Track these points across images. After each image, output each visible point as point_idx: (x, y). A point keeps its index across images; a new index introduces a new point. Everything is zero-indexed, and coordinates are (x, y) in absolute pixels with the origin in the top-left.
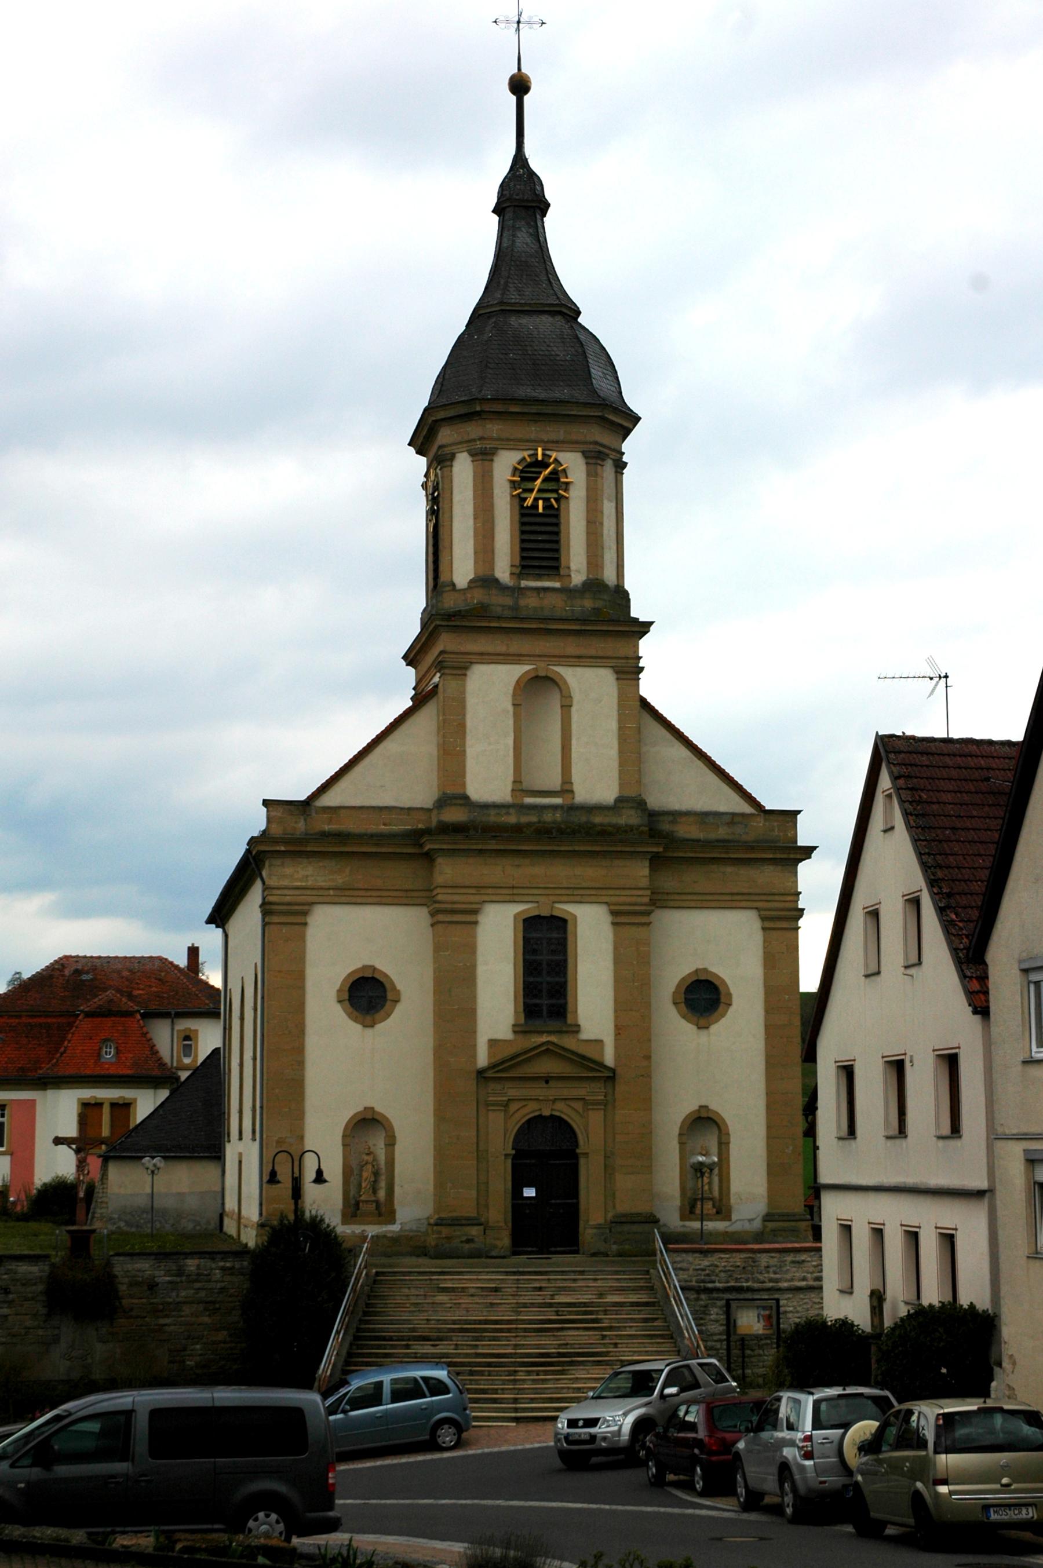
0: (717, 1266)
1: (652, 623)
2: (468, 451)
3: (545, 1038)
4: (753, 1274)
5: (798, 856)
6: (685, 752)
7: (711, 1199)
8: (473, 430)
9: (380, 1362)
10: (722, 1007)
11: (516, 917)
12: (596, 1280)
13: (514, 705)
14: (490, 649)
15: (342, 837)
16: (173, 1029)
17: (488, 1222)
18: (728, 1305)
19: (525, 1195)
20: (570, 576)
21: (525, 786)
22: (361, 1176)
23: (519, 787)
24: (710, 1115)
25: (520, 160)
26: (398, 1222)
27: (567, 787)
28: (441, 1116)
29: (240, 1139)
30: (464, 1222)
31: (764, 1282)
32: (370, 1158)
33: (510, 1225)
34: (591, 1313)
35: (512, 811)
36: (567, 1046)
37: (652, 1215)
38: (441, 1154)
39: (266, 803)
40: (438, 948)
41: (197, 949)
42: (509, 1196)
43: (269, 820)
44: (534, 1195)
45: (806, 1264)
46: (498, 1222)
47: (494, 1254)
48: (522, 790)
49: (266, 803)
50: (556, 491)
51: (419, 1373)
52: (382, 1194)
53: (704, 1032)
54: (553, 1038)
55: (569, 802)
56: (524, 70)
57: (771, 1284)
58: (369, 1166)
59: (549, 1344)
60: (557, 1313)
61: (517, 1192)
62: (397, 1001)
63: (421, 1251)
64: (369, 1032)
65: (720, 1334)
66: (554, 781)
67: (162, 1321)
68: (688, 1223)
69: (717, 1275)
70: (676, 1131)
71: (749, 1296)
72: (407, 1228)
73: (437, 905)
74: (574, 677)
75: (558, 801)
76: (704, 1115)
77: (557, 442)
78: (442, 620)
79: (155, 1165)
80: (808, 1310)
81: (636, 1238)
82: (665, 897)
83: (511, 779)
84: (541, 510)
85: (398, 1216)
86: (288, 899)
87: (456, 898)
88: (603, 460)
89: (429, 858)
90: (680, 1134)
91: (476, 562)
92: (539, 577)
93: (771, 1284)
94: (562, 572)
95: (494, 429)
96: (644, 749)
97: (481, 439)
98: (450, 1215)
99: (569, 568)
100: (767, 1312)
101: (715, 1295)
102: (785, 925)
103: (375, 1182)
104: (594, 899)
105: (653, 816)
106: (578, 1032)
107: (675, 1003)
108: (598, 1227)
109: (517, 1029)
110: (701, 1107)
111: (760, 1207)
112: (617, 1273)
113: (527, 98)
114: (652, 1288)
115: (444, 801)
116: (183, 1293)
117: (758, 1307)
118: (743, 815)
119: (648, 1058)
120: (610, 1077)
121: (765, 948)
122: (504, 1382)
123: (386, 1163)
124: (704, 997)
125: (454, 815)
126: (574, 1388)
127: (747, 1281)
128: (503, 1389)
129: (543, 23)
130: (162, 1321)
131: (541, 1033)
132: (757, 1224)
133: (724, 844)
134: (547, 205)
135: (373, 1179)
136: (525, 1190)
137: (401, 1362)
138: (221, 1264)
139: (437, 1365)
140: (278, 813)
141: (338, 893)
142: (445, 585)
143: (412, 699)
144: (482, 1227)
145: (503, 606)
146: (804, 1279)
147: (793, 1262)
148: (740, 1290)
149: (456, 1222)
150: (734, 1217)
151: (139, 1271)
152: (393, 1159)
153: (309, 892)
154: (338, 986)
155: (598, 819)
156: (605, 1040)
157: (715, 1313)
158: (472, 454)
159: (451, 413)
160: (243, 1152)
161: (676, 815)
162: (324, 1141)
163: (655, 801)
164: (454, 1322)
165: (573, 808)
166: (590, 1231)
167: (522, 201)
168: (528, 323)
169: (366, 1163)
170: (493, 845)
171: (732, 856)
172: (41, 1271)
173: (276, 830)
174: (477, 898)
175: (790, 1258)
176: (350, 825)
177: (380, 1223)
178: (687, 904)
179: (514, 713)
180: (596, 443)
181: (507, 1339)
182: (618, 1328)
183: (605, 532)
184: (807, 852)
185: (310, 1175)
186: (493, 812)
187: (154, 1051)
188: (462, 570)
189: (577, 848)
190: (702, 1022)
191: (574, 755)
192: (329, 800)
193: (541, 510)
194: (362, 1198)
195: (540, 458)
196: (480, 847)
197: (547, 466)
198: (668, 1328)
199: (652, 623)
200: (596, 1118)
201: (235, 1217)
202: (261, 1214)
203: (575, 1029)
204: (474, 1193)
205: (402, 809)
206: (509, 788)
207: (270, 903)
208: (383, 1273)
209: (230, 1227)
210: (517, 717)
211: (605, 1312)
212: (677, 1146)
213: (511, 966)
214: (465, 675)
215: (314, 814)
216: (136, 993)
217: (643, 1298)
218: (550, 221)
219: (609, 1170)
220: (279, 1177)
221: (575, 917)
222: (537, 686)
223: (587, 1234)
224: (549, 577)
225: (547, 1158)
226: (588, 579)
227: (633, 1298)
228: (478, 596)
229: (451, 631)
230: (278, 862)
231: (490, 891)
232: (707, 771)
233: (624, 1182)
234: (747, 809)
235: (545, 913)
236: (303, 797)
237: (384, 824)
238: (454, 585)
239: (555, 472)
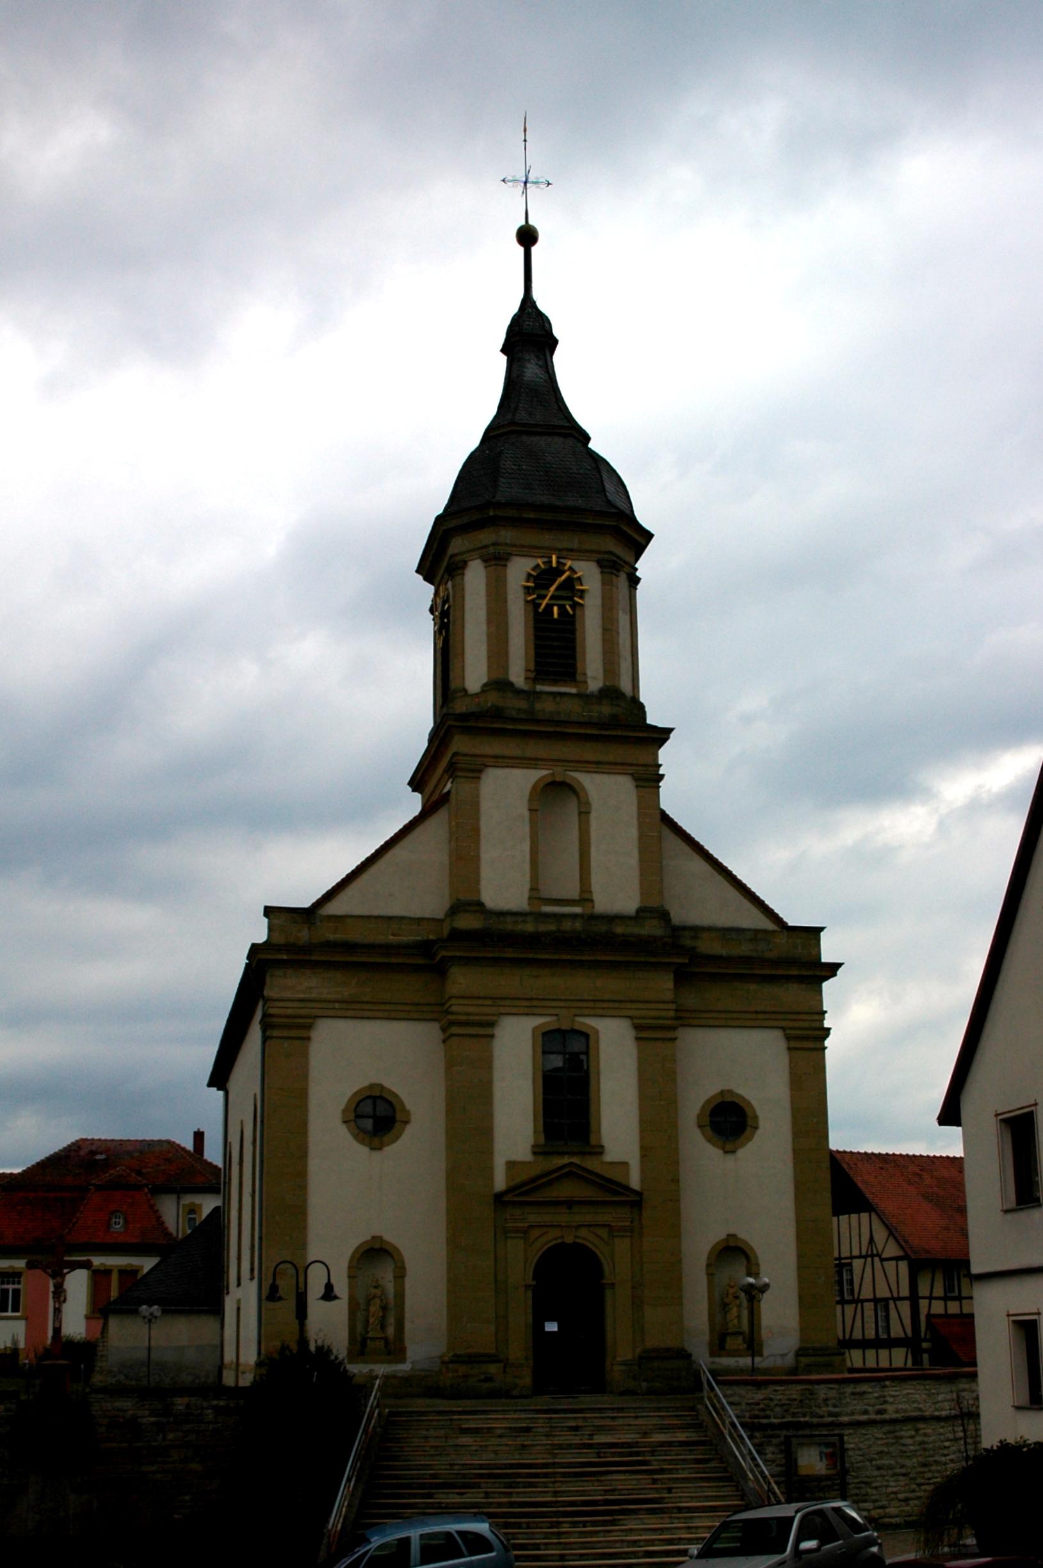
0: (771, 1399)
1: (672, 730)
2: (480, 557)
3: (566, 1160)
4: (810, 1407)
5: (823, 974)
6: (706, 867)
7: (740, 1333)
8: (485, 537)
9: (399, 1514)
10: (748, 1131)
11: (534, 1030)
12: (637, 1417)
13: (530, 810)
14: (506, 752)
15: (350, 947)
16: (178, 1204)
18: (787, 1442)
19: (547, 1329)
20: (586, 682)
21: (545, 894)
22: (367, 1310)
23: (535, 895)
24: (740, 1245)
25: (528, 302)
26: (409, 1361)
27: (586, 896)
28: (453, 1243)
29: (239, 1285)
31: (823, 1417)
32: (378, 1292)
34: (638, 1454)
35: (529, 919)
36: (589, 1167)
37: (683, 1350)
38: (454, 1284)
39: (269, 911)
40: (450, 1064)
41: (203, 1133)
43: (271, 929)
44: (556, 1329)
45: (866, 1396)
47: (515, 1393)
48: (540, 899)
49: (269, 911)
50: (571, 598)
51: (454, 1527)
52: (391, 1331)
53: (730, 1157)
54: (576, 1160)
55: (588, 911)
56: (531, 222)
57: (830, 1419)
58: (377, 1301)
59: (593, 1490)
60: (599, 1455)
61: (538, 1326)
62: (407, 1122)
63: (434, 1391)
64: (376, 1155)
66: (574, 892)
67: (146, 1468)
68: (717, 1360)
70: (703, 1261)
71: (807, 1432)
73: (451, 1017)
74: (594, 785)
75: (577, 910)
76: (732, 1244)
77: (572, 550)
78: (456, 720)
79: (151, 1314)
80: (870, 1446)
81: (669, 1376)
82: (688, 1015)
83: (527, 886)
84: (556, 616)
85: (409, 1354)
86: (289, 1012)
87: (471, 1009)
88: (618, 571)
89: (440, 970)
91: (489, 667)
92: (555, 682)
93: (830, 1419)
94: (579, 678)
95: (507, 535)
96: (664, 862)
97: (494, 544)
98: (468, 1351)
99: (585, 674)
100: (830, 1450)
102: (811, 1045)
103: (383, 1317)
104: (615, 1013)
105: (678, 931)
106: (601, 1153)
107: (700, 1126)
108: (624, 1363)
109: (538, 1150)
110: (729, 1235)
111: (791, 1342)
112: (659, 1409)
113: (534, 250)
115: (457, 908)
116: (171, 1436)
117: (820, 1444)
118: (765, 931)
119: (676, 1181)
120: (635, 1201)
121: (791, 1068)
122: (547, 1535)
123: (395, 1296)
124: (729, 1121)
125: (468, 922)
126: (628, 1541)
127: (804, 1415)
128: (546, 1544)
129: (549, 184)
130: (146, 1468)
131: (562, 1154)
132: (790, 1360)
133: (746, 960)
134: (556, 342)
135: (381, 1314)
136: (546, 1324)
137: (424, 1514)
138: (215, 1402)
139: (477, 1517)
140: (279, 921)
141: (344, 1006)
142: (456, 691)
143: (504, 350)
144: (502, 1365)
145: (519, 710)
146: (866, 1412)
147: (853, 1394)
149: (472, 1359)
150: (766, 1352)
151: (119, 1410)
152: (403, 1290)
153: (313, 1005)
154: (342, 1106)
155: (619, 930)
158: (486, 561)
159: (465, 520)
160: (243, 1297)
161: (696, 931)
162: (329, 1248)
163: (680, 915)
164: (481, 1467)
165: (593, 918)
166: (617, 1368)
167: (529, 338)
168: (541, 442)
169: (374, 1297)
170: (510, 953)
172: (7, 1410)
173: (279, 939)
174: (493, 1010)
175: (849, 1389)
176: (356, 935)
177: (390, 1362)
178: (711, 1022)
179: (531, 819)
180: (611, 553)
181: (545, 1485)
182: (670, 1471)
183: (621, 642)
184: (833, 969)
185: (315, 1288)
186: (509, 919)
187: (161, 1224)
188: (475, 674)
189: (599, 958)
190: (729, 1147)
191: (593, 864)
192: (332, 909)
193: (556, 616)
194: (370, 1335)
195: (554, 565)
196: (496, 955)
197: (563, 572)
198: (725, 1470)
199: (672, 730)
200: (622, 1245)
201: (234, 1366)
202: (259, 1353)
203: (597, 1150)
204: (493, 1328)
205: (411, 919)
206: (526, 896)
207: (272, 1016)
208: (398, 1414)
209: (229, 1379)
210: (533, 823)
211: (653, 1453)
214: (479, 778)
216: (144, 1171)
217: (692, 1436)
218: (559, 359)
220: (281, 1293)
221: (597, 1032)
222: (555, 792)
223: (616, 1372)
224: (565, 683)
225: (569, 1284)
226: (605, 685)
227: (682, 1437)
228: (493, 699)
229: (465, 732)
230: (279, 972)
231: (507, 1003)
232: (726, 884)
234: (770, 926)
235: (565, 1026)
236: (307, 904)
238: (465, 690)
239: (569, 579)
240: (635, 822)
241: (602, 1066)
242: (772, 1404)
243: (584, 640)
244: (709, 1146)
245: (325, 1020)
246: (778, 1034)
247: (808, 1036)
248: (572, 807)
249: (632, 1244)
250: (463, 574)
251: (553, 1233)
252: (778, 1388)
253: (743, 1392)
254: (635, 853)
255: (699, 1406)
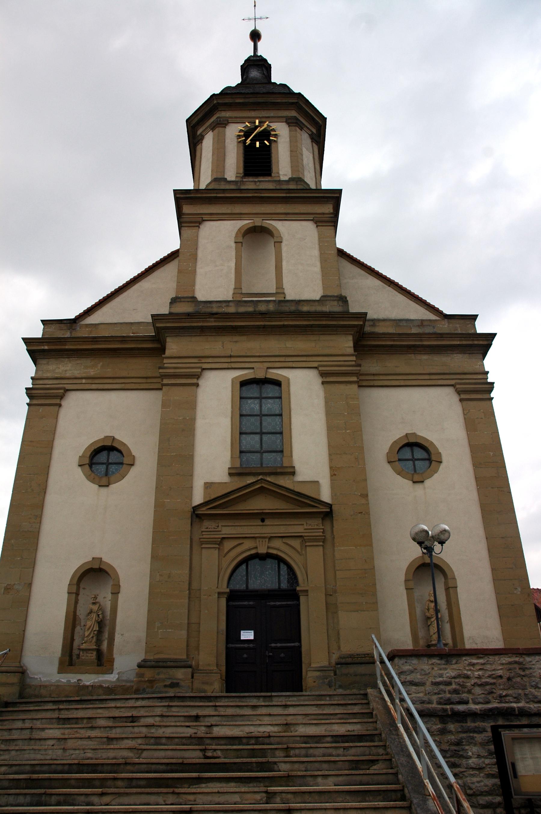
0: (468, 677)
6: (378, 283)
12: (286, 706)
17: (198, 665)
18: (497, 740)
19: (243, 638)
26: (115, 672)
27: (279, 291)
30: (169, 664)
33: (224, 669)
39: (44, 322)
42: (223, 637)
44: (252, 637)
46: (209, 665)
48: (242, 293)
49: (44, 322)
58: (94, 616)
61: (232, 635)
62: (114, 439)
64: (104, 490)
65: (489, 793)
69: (469, 692)
70: (402, 577)
72: (124, 678)
74: (282, 227)
76: (412, 440)
85: (116, 665)
90: (406, 581)
99: (278, 173)
101: (470, 724)
106: (293, 473)
113: (259, 44)
114: (370, 714)
118: (430, 320)
119: (365, 496)
120: (327, 513)
121: (464, 414)
124: (416, 456)
125: (183, 308)
127: (517, 699)
140: (52, 329)
141: (90, 381)
144: (190, 670)
148: (508, 713)
156: (321, 481)
157: (476, 754)
171: (425, 343)
183: (305, 162)
186: (214, 305)
192: (91, 320)
200: (314, 555)
204: (184, 633)
212: (405, 591)
213: (229, 420)
215: (78, 329)
217: (356, 728)
219: (331, 609)
221: (288, 380)
223: (310, 677)
227: (341, 729)
233: (347, 620)
234: (432, 317)
237: (133, 333)
240: (317, 246)
241: (293, 406)
242: (469, 684)
243: (278, 162)
244: (399, 479)
245: (73, 392)
246: (450, 391)
247: (477, 392)
248: (271, 248)
249: (324, 554)
250: (202, 143)
251: (248, 544)
252: (475, 661)
253: (426, 667)
254: (318, 264)
255: (369, 691)
